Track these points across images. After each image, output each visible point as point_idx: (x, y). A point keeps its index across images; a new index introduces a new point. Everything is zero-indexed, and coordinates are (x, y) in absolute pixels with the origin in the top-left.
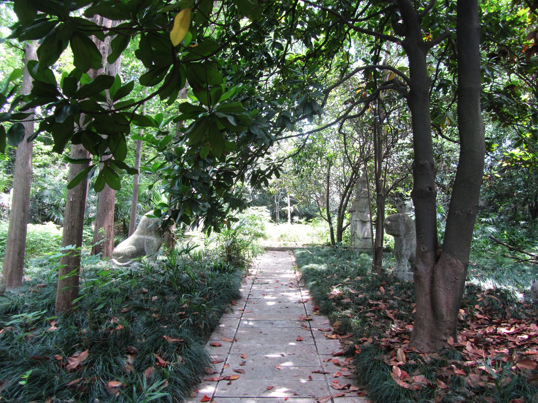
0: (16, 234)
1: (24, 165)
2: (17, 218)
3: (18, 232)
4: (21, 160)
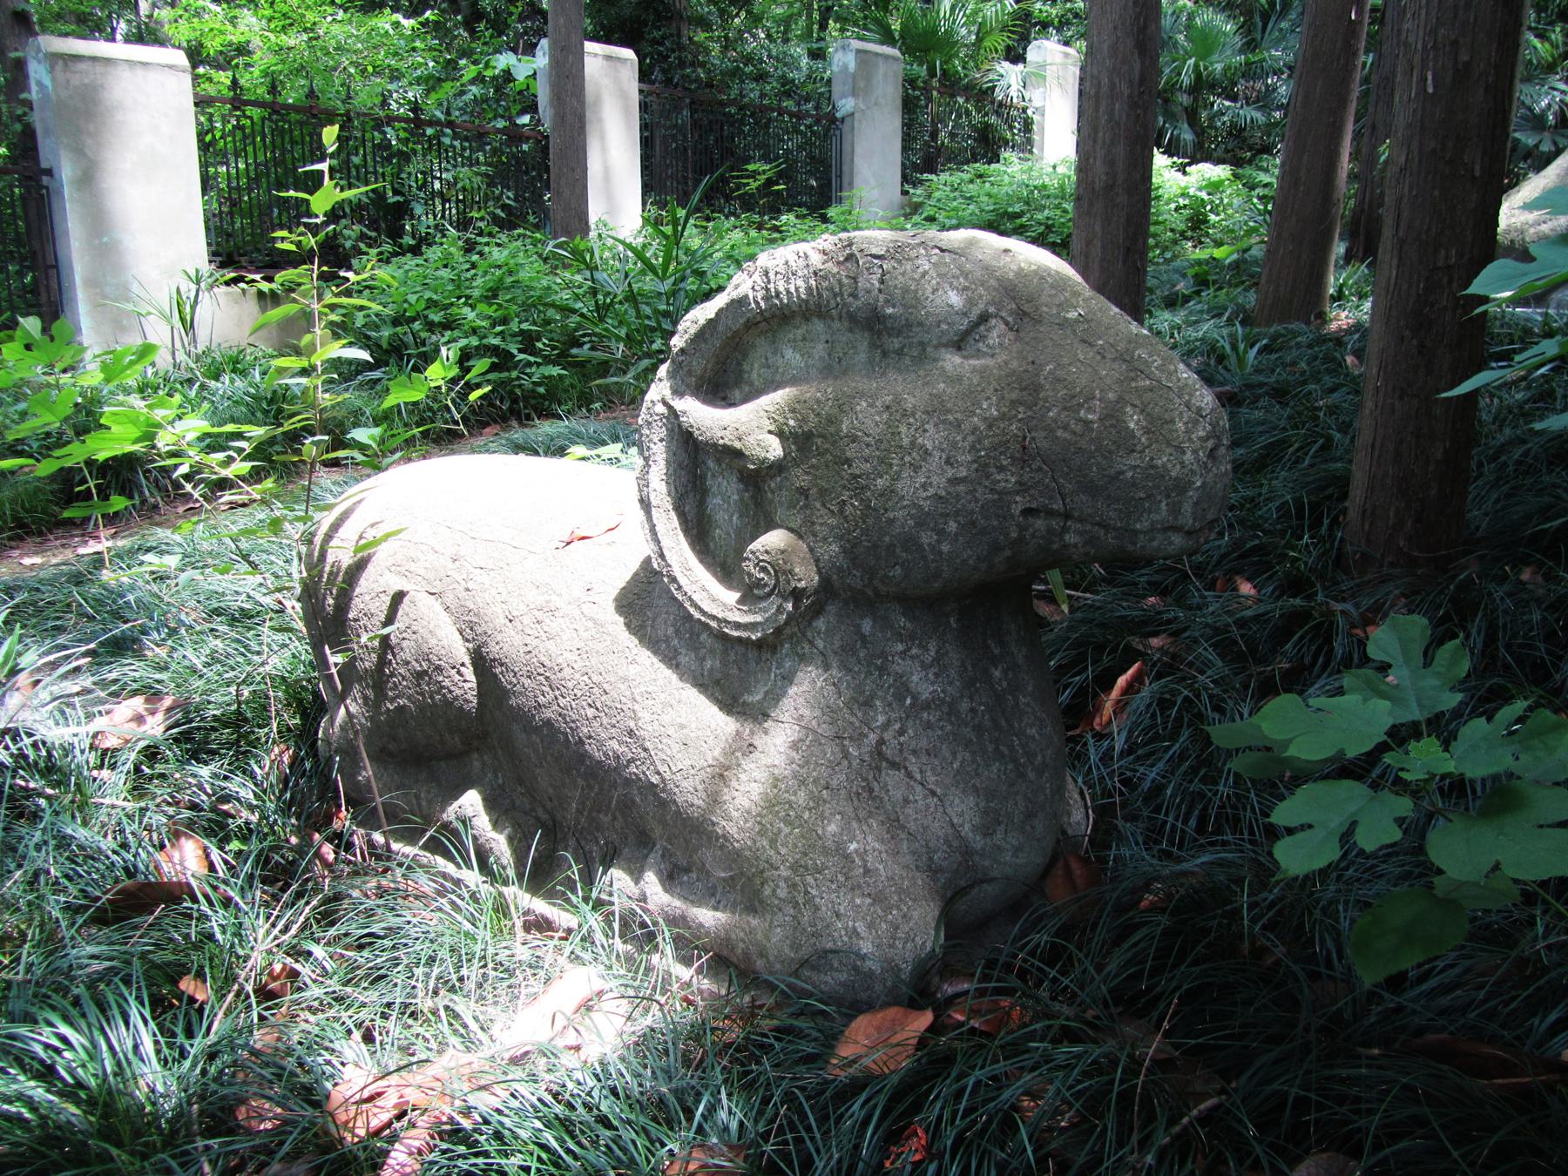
0: (1111, 162)
2: (1112, 86)
3: (1121, 151)
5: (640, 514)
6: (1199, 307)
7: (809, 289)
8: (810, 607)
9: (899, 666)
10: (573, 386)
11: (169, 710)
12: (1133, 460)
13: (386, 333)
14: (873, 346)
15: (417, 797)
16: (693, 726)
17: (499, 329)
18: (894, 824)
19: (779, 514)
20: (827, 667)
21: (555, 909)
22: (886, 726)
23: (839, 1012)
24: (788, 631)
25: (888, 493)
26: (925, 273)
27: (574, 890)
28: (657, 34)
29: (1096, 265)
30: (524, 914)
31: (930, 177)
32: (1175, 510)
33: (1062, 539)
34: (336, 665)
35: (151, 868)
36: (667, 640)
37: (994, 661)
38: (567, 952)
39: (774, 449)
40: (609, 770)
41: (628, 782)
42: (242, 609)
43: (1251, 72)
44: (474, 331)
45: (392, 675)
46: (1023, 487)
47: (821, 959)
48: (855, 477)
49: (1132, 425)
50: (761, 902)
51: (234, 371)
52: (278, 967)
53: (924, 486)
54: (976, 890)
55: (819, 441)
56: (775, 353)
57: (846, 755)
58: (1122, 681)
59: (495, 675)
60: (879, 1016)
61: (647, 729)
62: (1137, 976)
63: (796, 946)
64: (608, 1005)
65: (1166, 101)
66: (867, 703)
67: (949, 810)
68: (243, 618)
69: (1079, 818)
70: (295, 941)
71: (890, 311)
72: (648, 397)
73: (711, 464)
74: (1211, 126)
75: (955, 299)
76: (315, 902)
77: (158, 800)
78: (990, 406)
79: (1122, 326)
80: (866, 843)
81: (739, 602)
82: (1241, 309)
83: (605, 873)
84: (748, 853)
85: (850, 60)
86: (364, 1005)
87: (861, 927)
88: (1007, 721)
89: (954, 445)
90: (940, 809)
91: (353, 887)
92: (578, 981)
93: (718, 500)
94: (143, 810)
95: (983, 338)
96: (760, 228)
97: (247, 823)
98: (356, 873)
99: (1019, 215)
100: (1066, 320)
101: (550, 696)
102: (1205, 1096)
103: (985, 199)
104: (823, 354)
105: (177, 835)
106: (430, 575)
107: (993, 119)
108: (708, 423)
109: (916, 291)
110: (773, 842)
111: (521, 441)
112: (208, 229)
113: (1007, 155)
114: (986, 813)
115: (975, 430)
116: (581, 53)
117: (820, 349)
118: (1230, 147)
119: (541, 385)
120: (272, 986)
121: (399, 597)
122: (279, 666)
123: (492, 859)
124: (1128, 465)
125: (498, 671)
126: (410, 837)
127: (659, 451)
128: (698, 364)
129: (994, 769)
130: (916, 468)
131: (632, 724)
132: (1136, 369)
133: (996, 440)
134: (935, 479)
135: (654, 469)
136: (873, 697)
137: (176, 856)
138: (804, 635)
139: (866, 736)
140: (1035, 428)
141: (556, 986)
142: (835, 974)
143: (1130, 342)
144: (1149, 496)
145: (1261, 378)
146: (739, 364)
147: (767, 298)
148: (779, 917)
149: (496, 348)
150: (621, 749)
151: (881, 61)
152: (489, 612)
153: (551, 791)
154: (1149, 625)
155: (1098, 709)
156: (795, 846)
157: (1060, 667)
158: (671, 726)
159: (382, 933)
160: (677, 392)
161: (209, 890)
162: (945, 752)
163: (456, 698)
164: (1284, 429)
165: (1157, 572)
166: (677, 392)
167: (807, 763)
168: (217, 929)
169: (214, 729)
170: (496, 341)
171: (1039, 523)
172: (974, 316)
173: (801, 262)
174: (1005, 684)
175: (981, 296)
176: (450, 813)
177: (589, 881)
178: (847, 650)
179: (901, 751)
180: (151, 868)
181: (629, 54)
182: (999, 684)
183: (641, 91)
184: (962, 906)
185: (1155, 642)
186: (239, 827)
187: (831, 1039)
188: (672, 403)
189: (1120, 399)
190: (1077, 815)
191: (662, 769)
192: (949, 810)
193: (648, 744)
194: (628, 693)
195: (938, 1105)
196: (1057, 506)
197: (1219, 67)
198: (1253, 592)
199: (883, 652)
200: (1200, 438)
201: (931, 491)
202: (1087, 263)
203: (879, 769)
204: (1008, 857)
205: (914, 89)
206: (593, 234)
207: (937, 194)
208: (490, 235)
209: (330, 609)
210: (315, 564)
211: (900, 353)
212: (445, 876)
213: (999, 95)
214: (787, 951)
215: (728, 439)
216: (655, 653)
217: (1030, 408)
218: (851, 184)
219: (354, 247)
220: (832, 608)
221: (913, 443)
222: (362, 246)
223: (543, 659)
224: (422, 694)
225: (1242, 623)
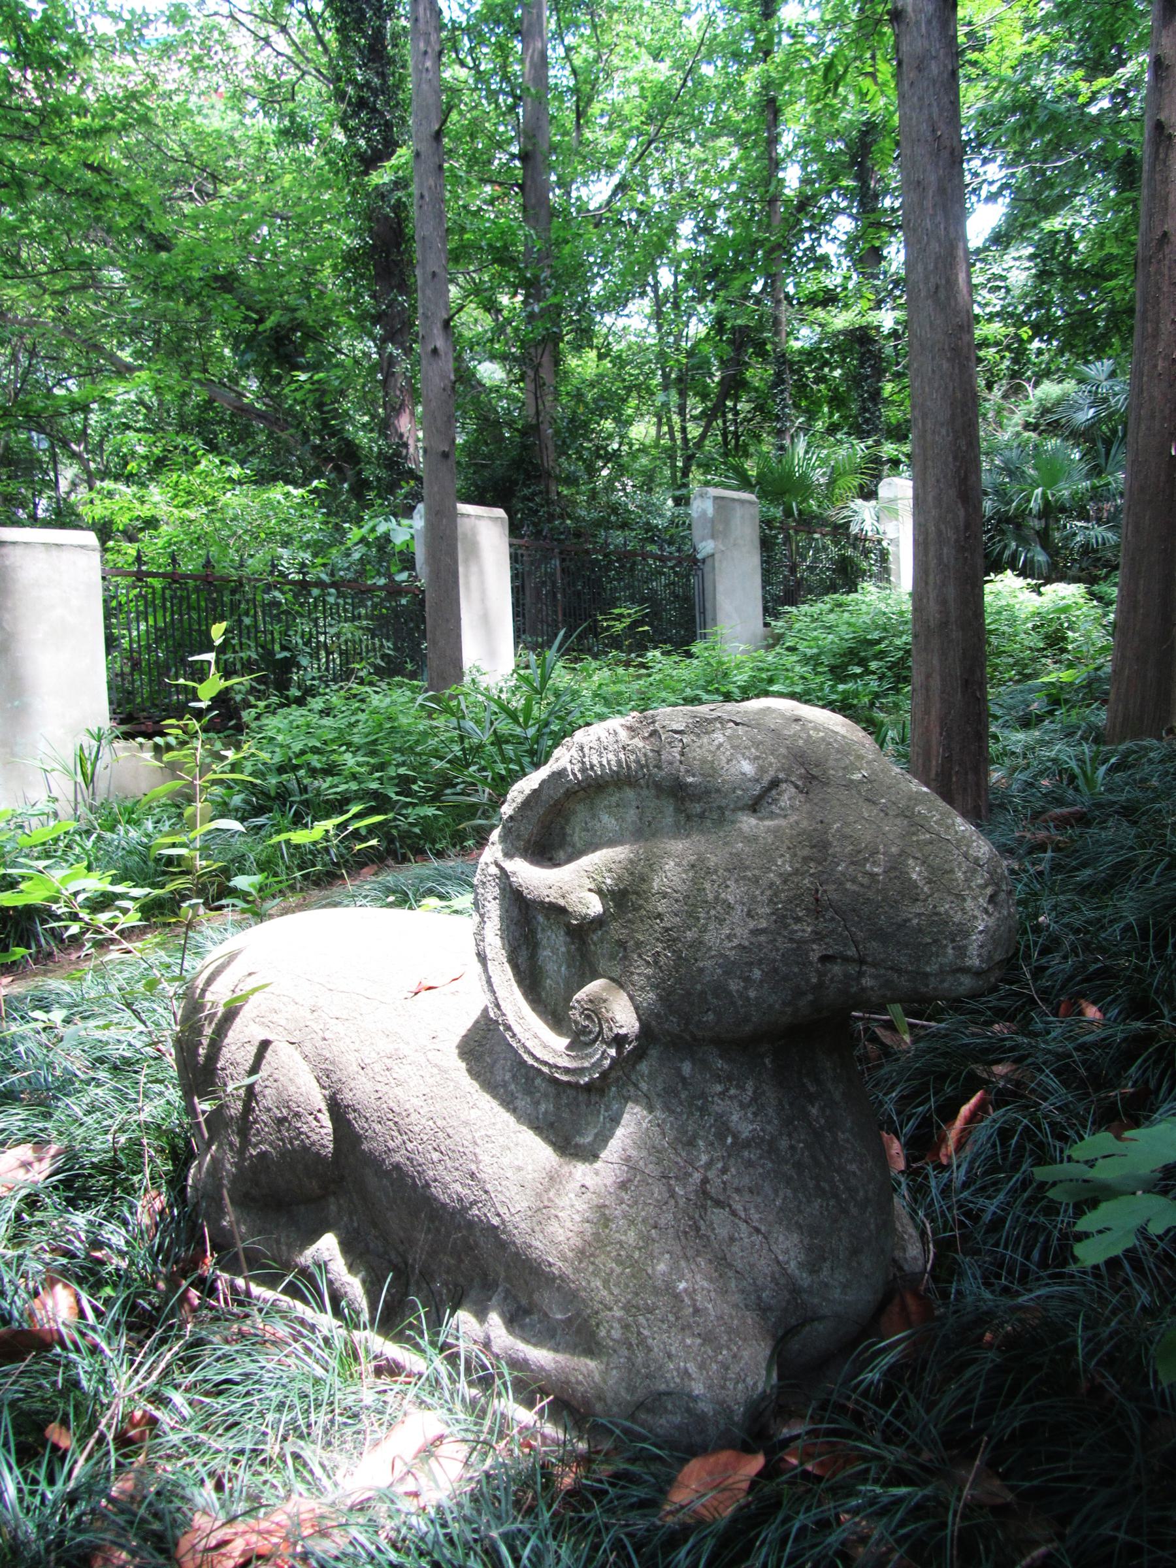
0: (943, 602)
1: (942, 295)
2: (939, 533)
3: (951, 592)
4: (927, 278)
5: (478, 967)
6: (1052, 727)
7: (619, 762)
8: (633, 1054)
9: (719, 1106)
10: (447, 825)
11: (54, 1157)
12: (918, 908)
13: (273, 781)
14: (678, 811)
15: (278, 1242)
16: (530, 1168)
17: (378, 775)
18: (722, 1263)
19: (602, 965)
20: (651, 1109)
21: (406, 1353)
22: (709, 1165)
23: (671, 1456)
24: (613, 1075)
25: (697, 944)
26: (721, 745)
27: (422, 1335)
28: (526, 492)
29: (937, 698)
30: (375, 1357)
31: (790, 609)
32: (962, 951)
33: (859, 983)
34: (204, 1112)
35: (26, 1315)
36: (505, 1085)
37: (811, 1099)
38: (410, 1396)
39: (595, 906)
40: (454, 1213)
41: (470, 1225)
42: (124, 1057)
43: (1096, 494)
44: (354, 777)
45: (256, 1121)
46: (818, 937)
47: (654, 1402)
48: (667, 930)
49: (914, 876)
50: (598, 1344)
51: (128, 822)
52: (138, 1414)
53: (729, 937)
54: (808, 1328)
55: (634, 897)
56: (593, 817)
57: (673, 1194)
58: (965, 1110)
59: (349, 1121)
60: (712, 1460)
61: (487, 1172)
62: (965, 1417)
63: (631, 1389)
64: (446, 1449)
65: (1018, 527)
66: (691, 1143)
67: (775, 1248)
68: (122, 1068)
69: (915, 1253)
70: (156, 1388)
71: (690, 780)
72: (482, 859)
73: (541, 919)
74: (1065, 547)
75: (747, 767)
76: (176, 1349)
77: (37, 1247)
78: (784, 863)
79: (902, 785)
80: (694, 1282)
81: (568, 1048)
82: (1091, 727)
83: (452, 1315)
84: (583, 1294)
85: (708, 507)
86: (218, 1451)
87: (692, 1367)
88: (827, 1157)
89: (753, 899)
90: (765, 1246)
91: (214, 1333)
92: (422, 1423)
93: (547, 953)
94: (21, 1257)
95: (775, 801)
96: (627, 664)
97: (117, 1270)
98: (217, 1319)
99: (878, 642)
100: (852, 781)
101: (399, 1141)
102: (1035, 1544)
103: (844, 628)
104: (635, 818)
105: (51, 1283)
106: (290, 1026)
107: (850, 552)
108: (535, 883)
109: (712, 762)
110: (606, 1283)
111: (391, 885)
112: (110, 688)
113: (865, 585)
114: (810, 1249)
115: (771, 885)
116: (454, 515)
117: (632, 815)
118: (1084, 565)
119: (404, 833)
120: (132, 1433)
121: (265, 1045)
122: (155, 1112)
123: (343, 1303)
124: (913, 912)
125: (351, 1116)
126: (270, 1281)
127: (493, 909)
128: (527, 829)
129: (816, 1205)
130: (721, 921)
131: (473, 1167)
132: (915, 823)
133: (791, 894)
134: (738, 931)
135: (489, 925)
136: (695, 1136)
137: (50, 1303)
138: (629, 1078)
139: (691, 1175)
140: (827, 882)
141: (399, 1431)
142: (670, 1417)
143: (910, 799)
144: (935, 941)
145: (1111, 798)
146: (563, 828)
147: (583, 770)
148: (615, 1360)
149: (375, 792)
150: (464, 1192)
151: (737, 506)
152: (344, 1060)
153: (402, 1234)
154: (991, 1053)
155: (943, 1139)
156: (627, 1286)
157: (902, 1098)
158: (503, 1166)
159: (238, 1379)
160: (508, 855)
161: (77, 1336)
162: (767, 1188)
163: (313, 1144)
164: (1132, 848)
165: (1001, 999)
166: (508, 855)
167: (636, 1203)
168: (82, 1375)
169: (91, 1176)
170: (374, 786)
171: (837, 969)
172: (765, 782)
173: (612, 739)
174: (822, 1121)
175: (771, 764)
176: (307, 1257)
177: (436, 1322)
178: (669, 1093)
179: (725, 1189)
180: (26, 1315)
181: (500, 513)
182: (817, 1121)
183: (511, 545)
184: (795, 1345)
185: (999, 1069)
186: (109, 1273)
187: (664, 1485)
188: (504, 865)
189: (902, 853)
190: (914, 1250)
191: (502, 1210)
192: (774, 1247)
193: (488, 1187)
194: (469, 1137)
195: (764, 1551)
196: (851, 952)
197: (1066, 493)
198: (1098, 1015)
199: (703, 1093)
200: (979, 886)
201: (736, 942)
202: (928, 696)
203: (704, 1207)
204: (837, 1294)
205: (771, 529)
206: (467, 679)
207: (797, 626)
208: (371, 684)
209: (201, 1060)
210: (194, 1006)
211: (702, 816)
212: (302, 1322)
213: (854, 529)
214: (623, 1393)
215: (553, 897)
216: (494, 1097)
217: (820, 864)
218: (714, 619)
219: (244, 700)
220: (654, 1052)
221: (717, 898)
222: (251, 698)
223: (392, 1105)
224: (282, 1140)
225: (1083, 1048)
